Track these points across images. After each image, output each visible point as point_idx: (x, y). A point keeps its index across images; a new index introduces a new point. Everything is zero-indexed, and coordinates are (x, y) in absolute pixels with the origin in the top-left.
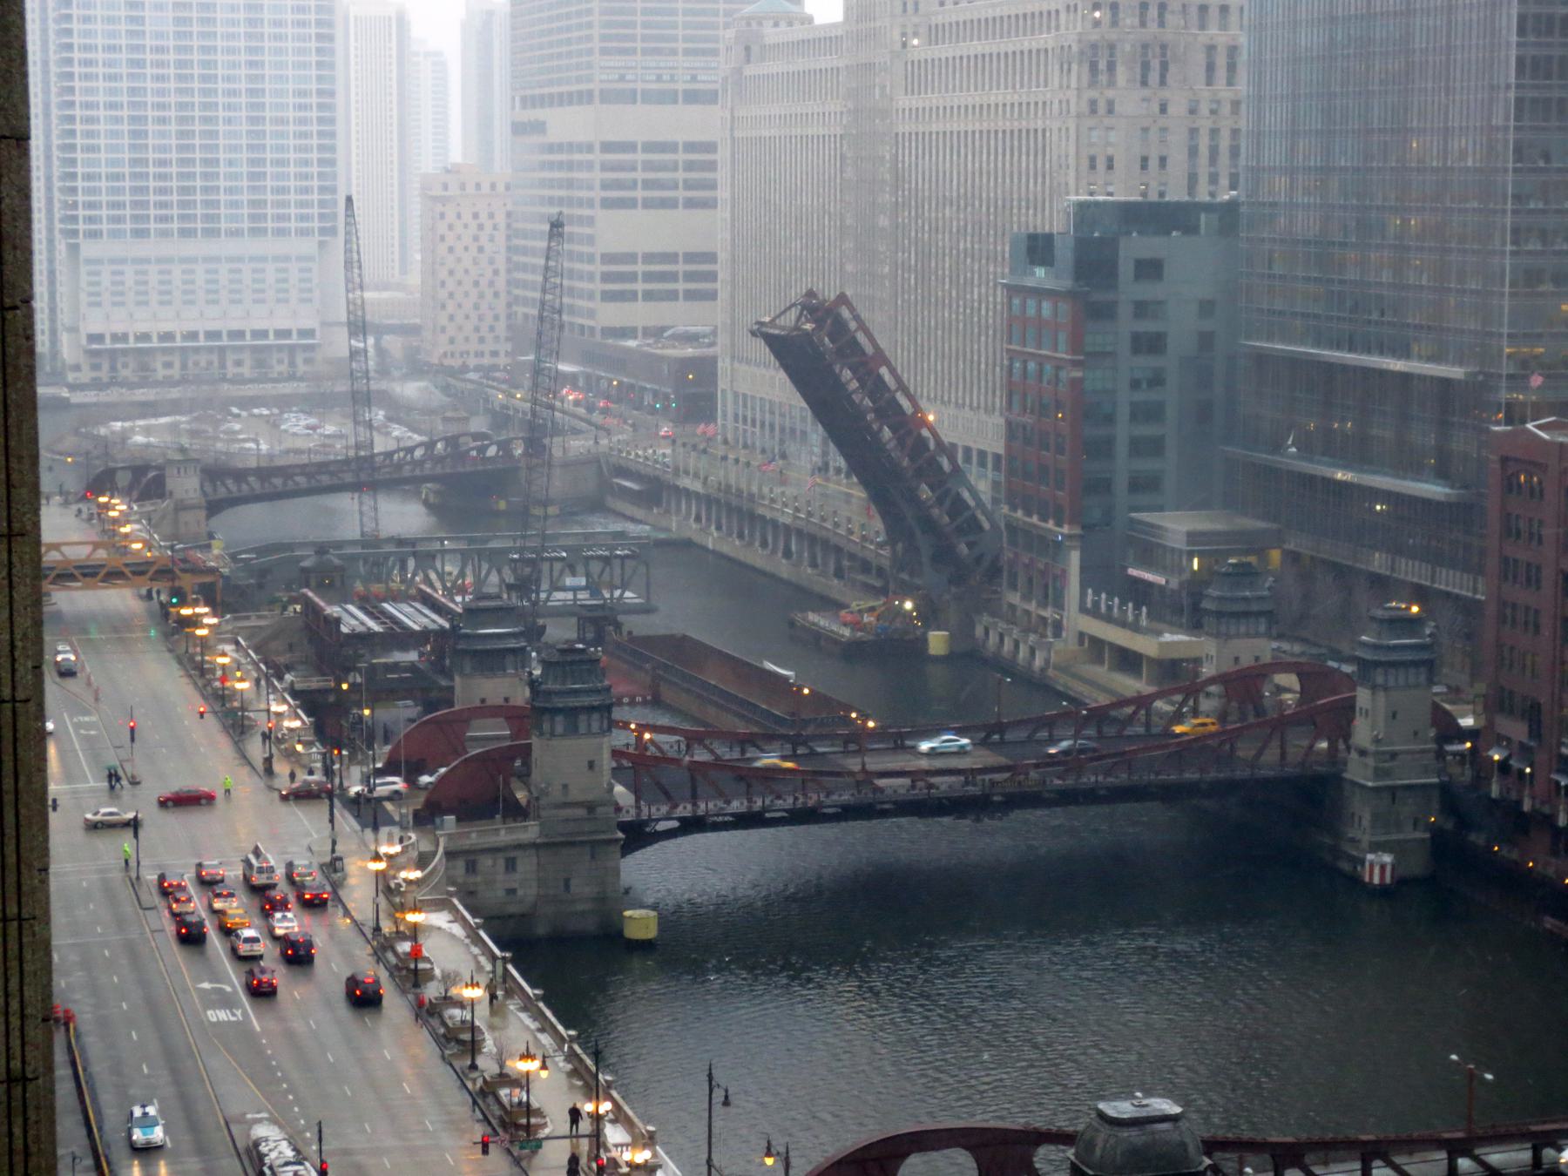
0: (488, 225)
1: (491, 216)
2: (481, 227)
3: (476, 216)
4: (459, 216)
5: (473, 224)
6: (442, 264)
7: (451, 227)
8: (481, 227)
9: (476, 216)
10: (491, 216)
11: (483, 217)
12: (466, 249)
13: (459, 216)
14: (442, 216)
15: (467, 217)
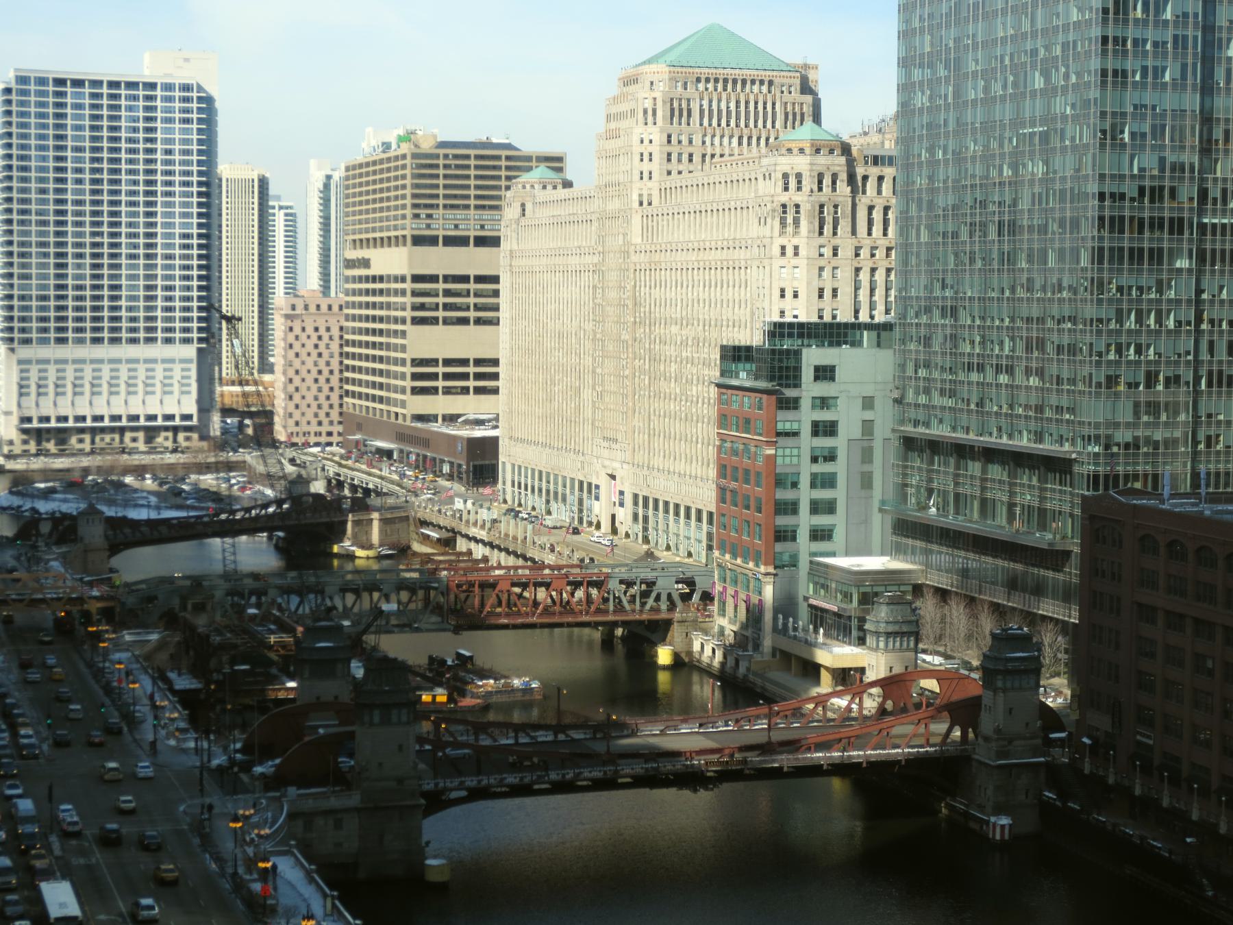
0: (326, 336)
1: (328, 329)
2: (320, 338)
3: (316, 329)
4: (303, 329)
5: (314, 336)
6: (291, 366)
8: (320, 338)
9: (316, 329)
10: (328, 329)
11: (322, 331)
12: (309, 354)
13: (303, 329)
14: (291, 329)
15: (310, 330)
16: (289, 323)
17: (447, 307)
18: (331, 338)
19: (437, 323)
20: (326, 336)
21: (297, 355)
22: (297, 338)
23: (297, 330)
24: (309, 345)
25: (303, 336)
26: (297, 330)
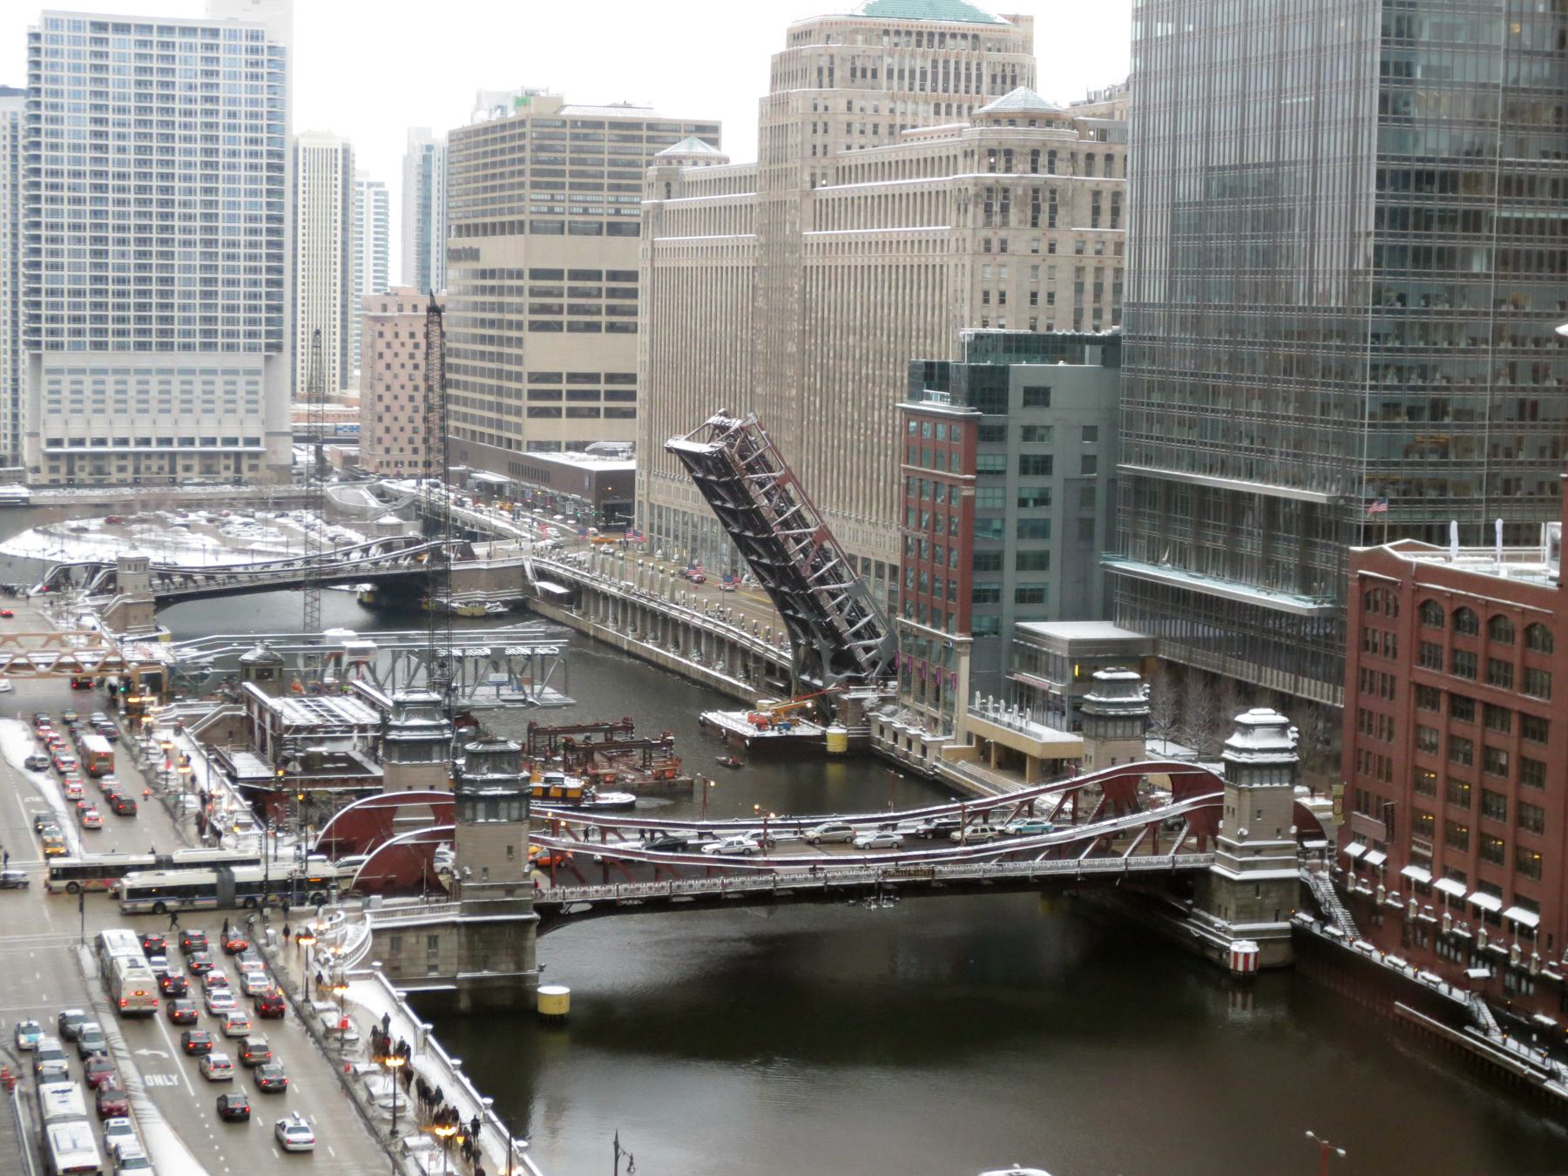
3: (412, 335)
4: (397, 335)
5: (410, 343)
7: (389, 345)
13: (397, 335)
14: (381, 335)
15: (404, 336)
16: (378, 327)
21: (388, 366)
23: (389, 336)
25: (396, 344)
26: (389, 336)
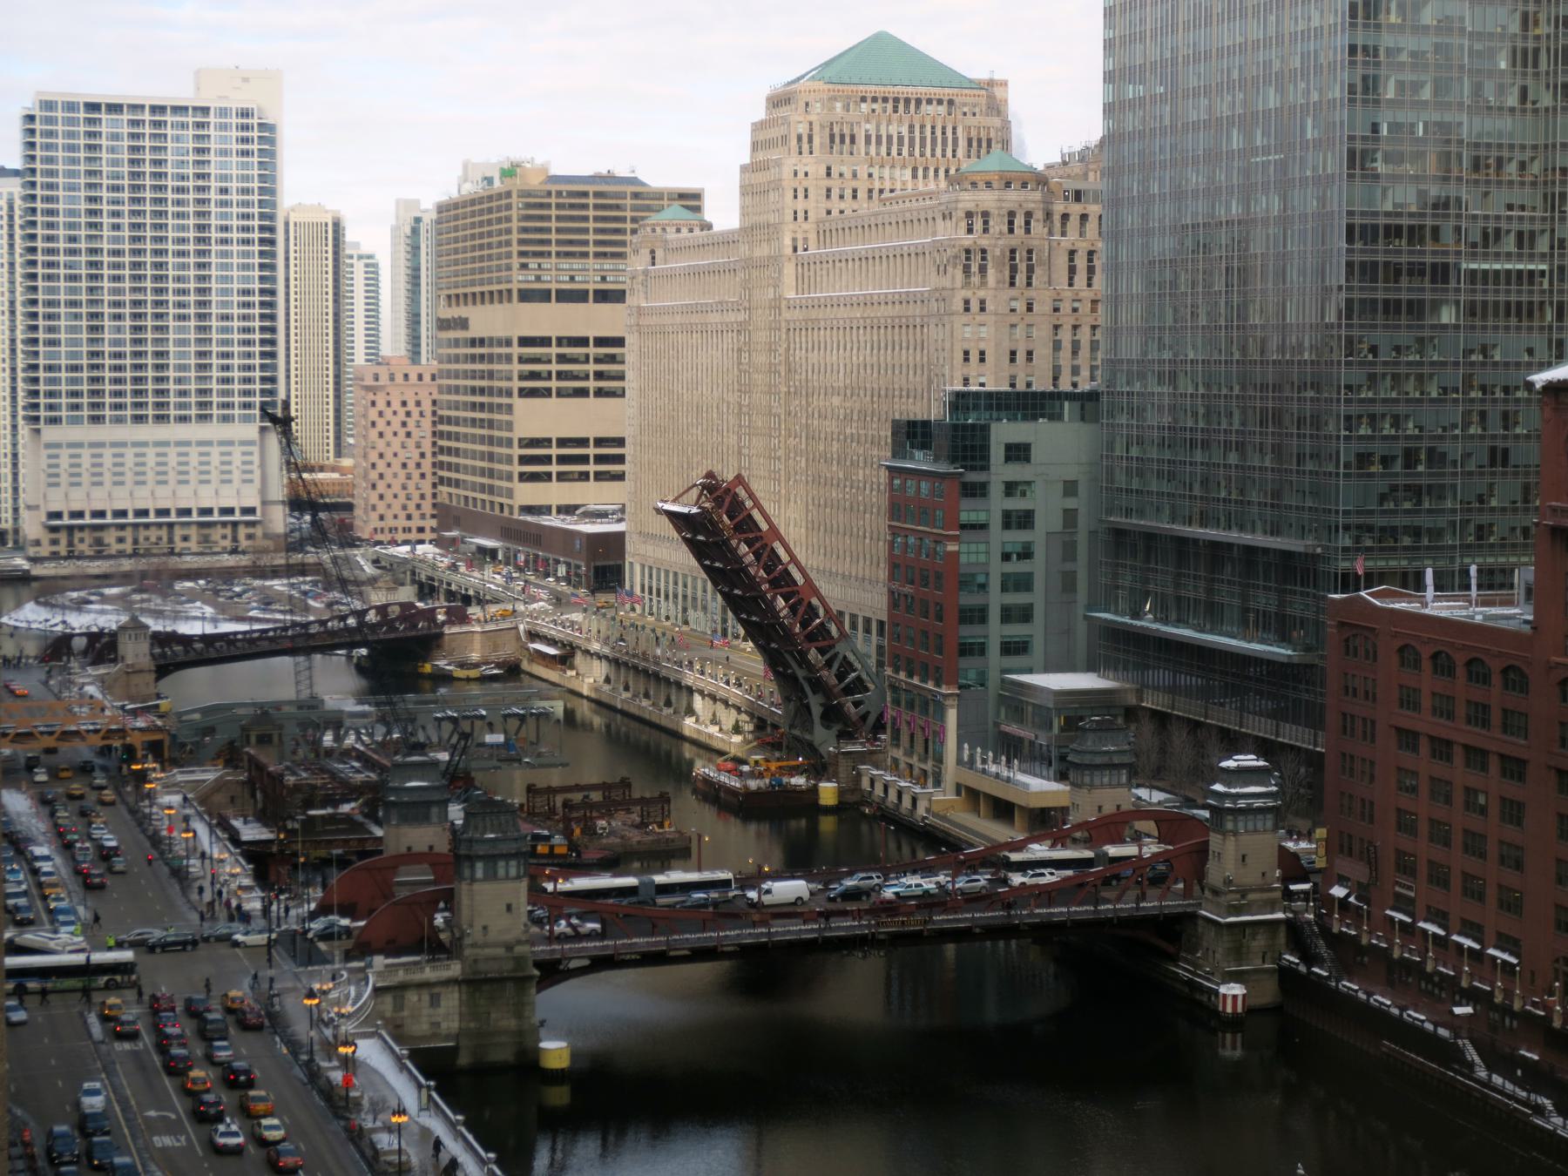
1: (418, 404)
2: (408, 414)
3: (404, 404)
4: (389, 404)
5: (402, 411)
7: (381, 414)
8: (408, 414)
9: (404, 404)
10: (418, 404)
11: (411, 406)
12: (395, 434)
13: (389, 404)
14: (373, 404)
15: (396, 405)
17: (561, 375)
18: (421, 414)
19: (550, 395)
20: (415, 412)
22: (381, 414)
23: (381, 405)
24: (396, 425)
25: (388, 412)
26: (381, 405)
